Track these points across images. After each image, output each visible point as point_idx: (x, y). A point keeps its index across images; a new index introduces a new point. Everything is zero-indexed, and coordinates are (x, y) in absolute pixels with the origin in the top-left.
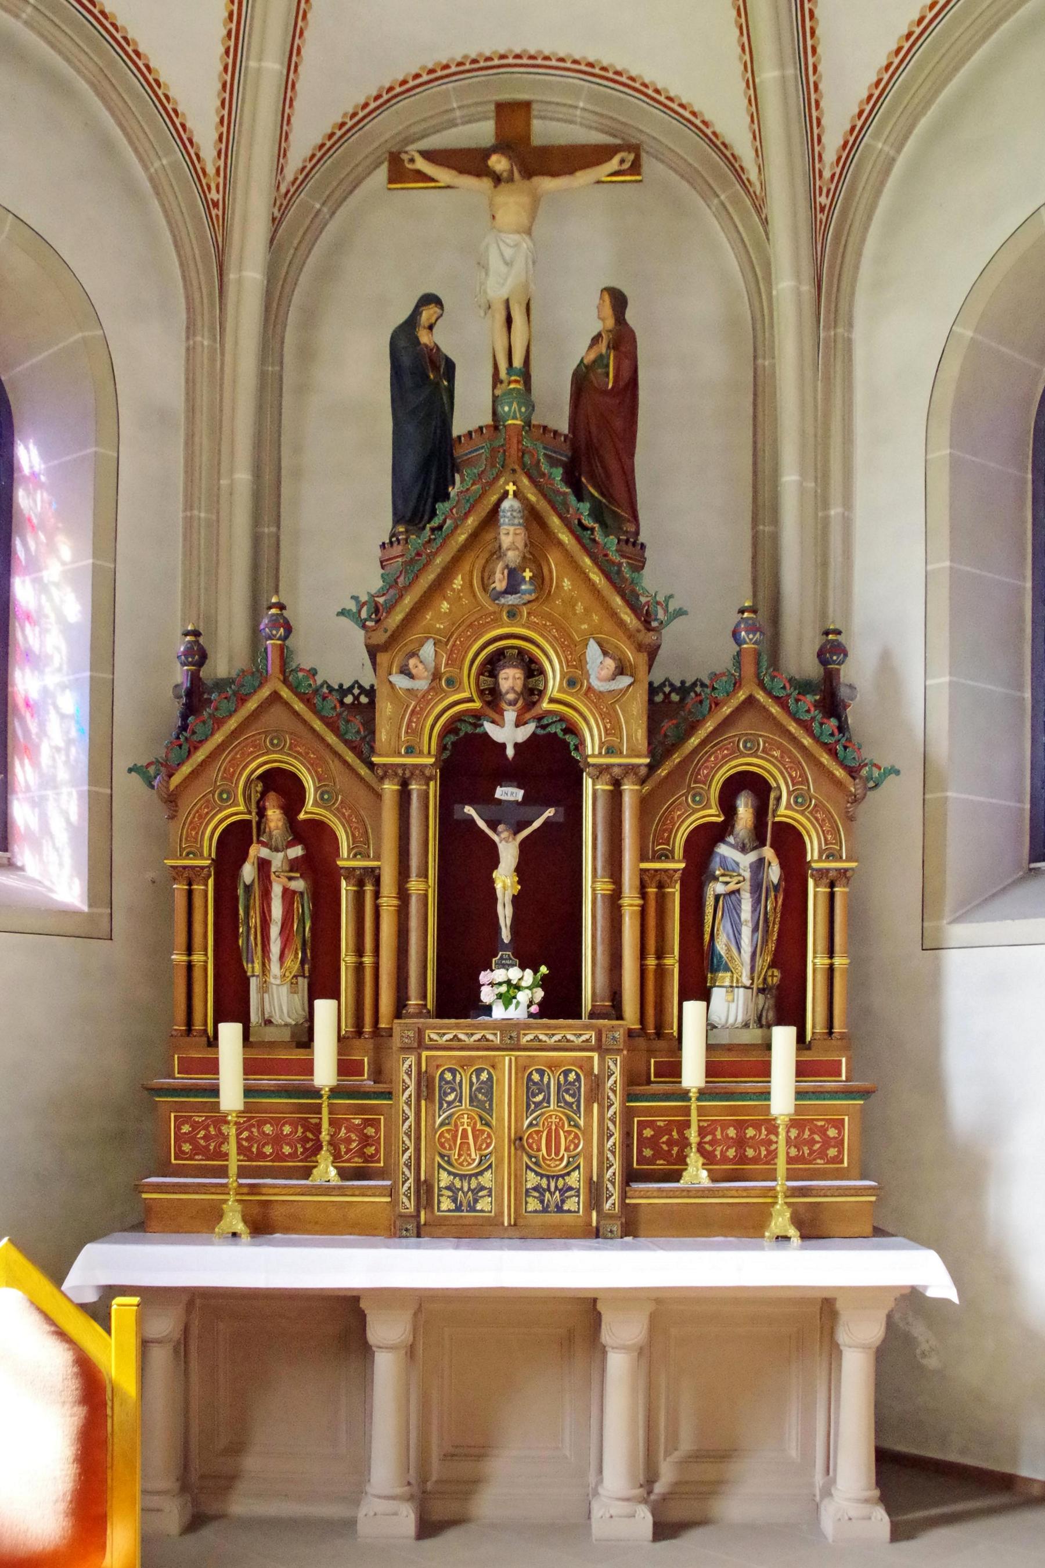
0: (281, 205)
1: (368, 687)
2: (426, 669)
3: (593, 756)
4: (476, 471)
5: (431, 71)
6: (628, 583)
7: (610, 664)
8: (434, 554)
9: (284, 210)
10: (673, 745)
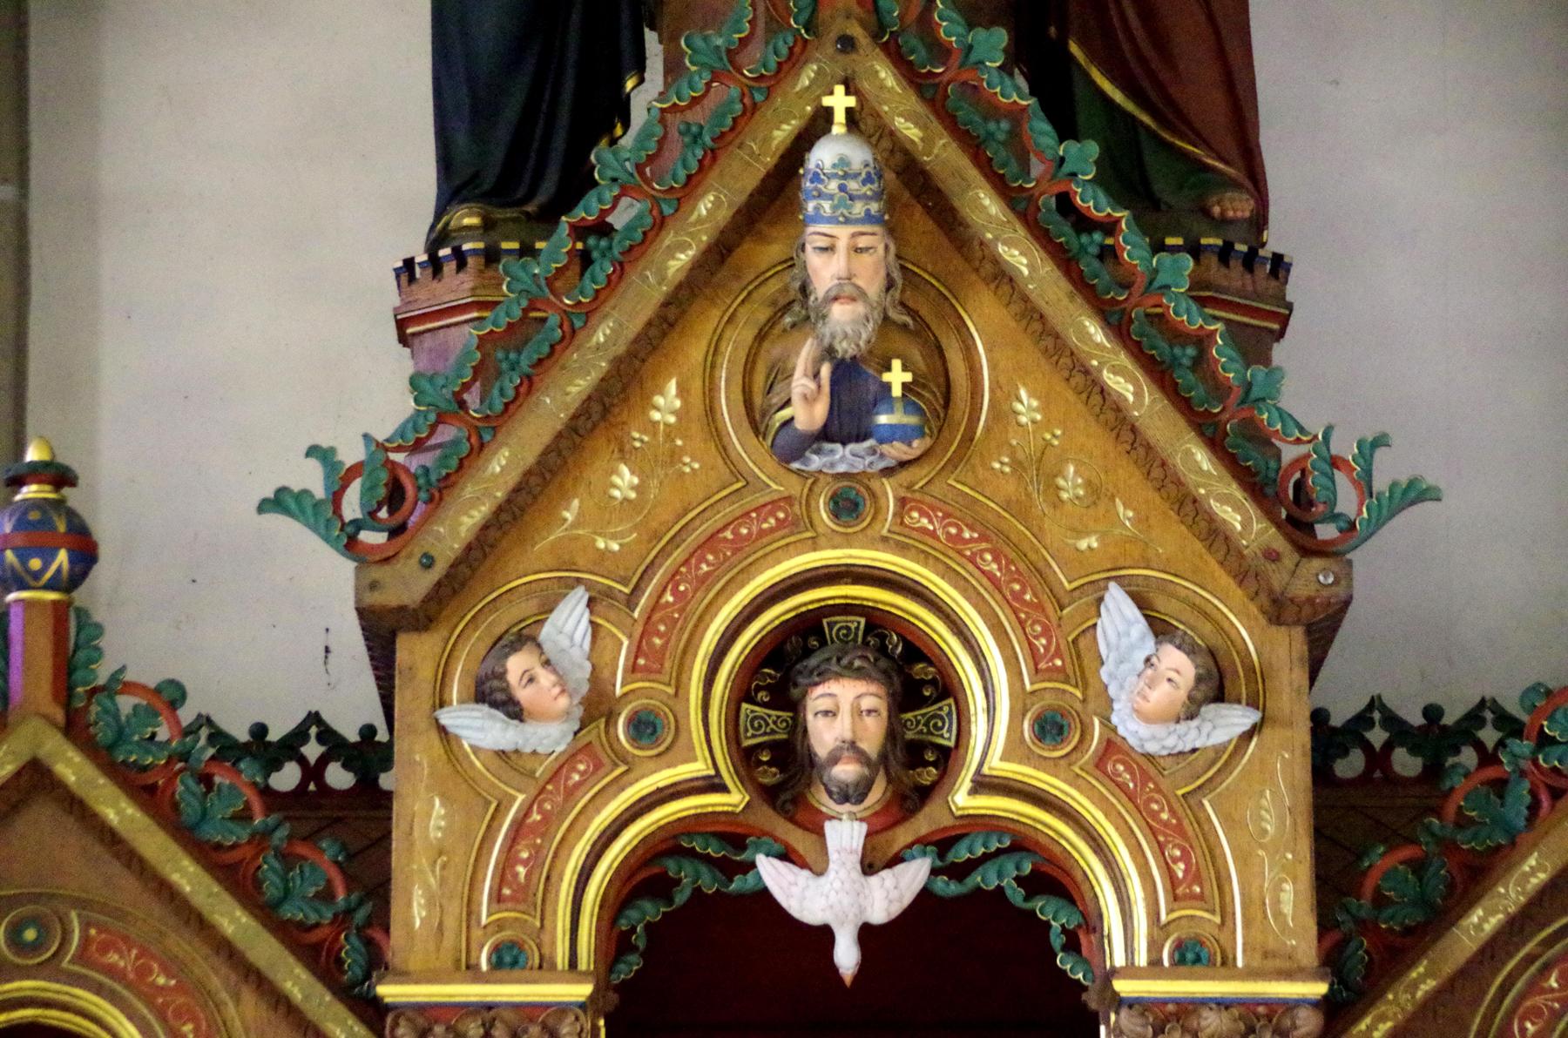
1: (353, 736)
3: (1131, 971)
7: (1178, 666)
8: (589, 313)
10: (1408, 931)
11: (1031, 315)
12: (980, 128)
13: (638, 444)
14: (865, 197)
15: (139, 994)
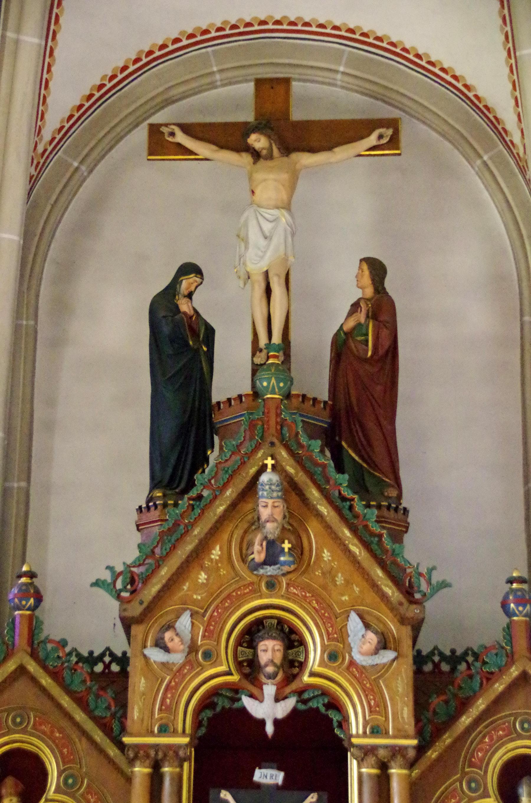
0: (38, 163)
1: (119, 654)
2: (182, 641)
3: (358, 736)
4: (234, 443)
5: (191, 36)
6: (390, 553)
7: (372, 638)
8: (193, 525)
9: (40, 168)
10: (444, 723)
11: (328, 527)
12: (313, 469)
13: (207, 565)
14: (277, 491)
15: (50, 738)
